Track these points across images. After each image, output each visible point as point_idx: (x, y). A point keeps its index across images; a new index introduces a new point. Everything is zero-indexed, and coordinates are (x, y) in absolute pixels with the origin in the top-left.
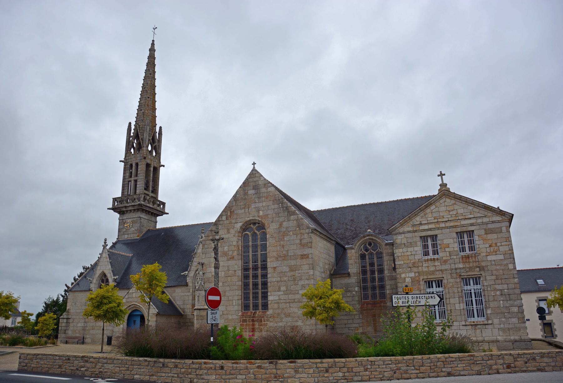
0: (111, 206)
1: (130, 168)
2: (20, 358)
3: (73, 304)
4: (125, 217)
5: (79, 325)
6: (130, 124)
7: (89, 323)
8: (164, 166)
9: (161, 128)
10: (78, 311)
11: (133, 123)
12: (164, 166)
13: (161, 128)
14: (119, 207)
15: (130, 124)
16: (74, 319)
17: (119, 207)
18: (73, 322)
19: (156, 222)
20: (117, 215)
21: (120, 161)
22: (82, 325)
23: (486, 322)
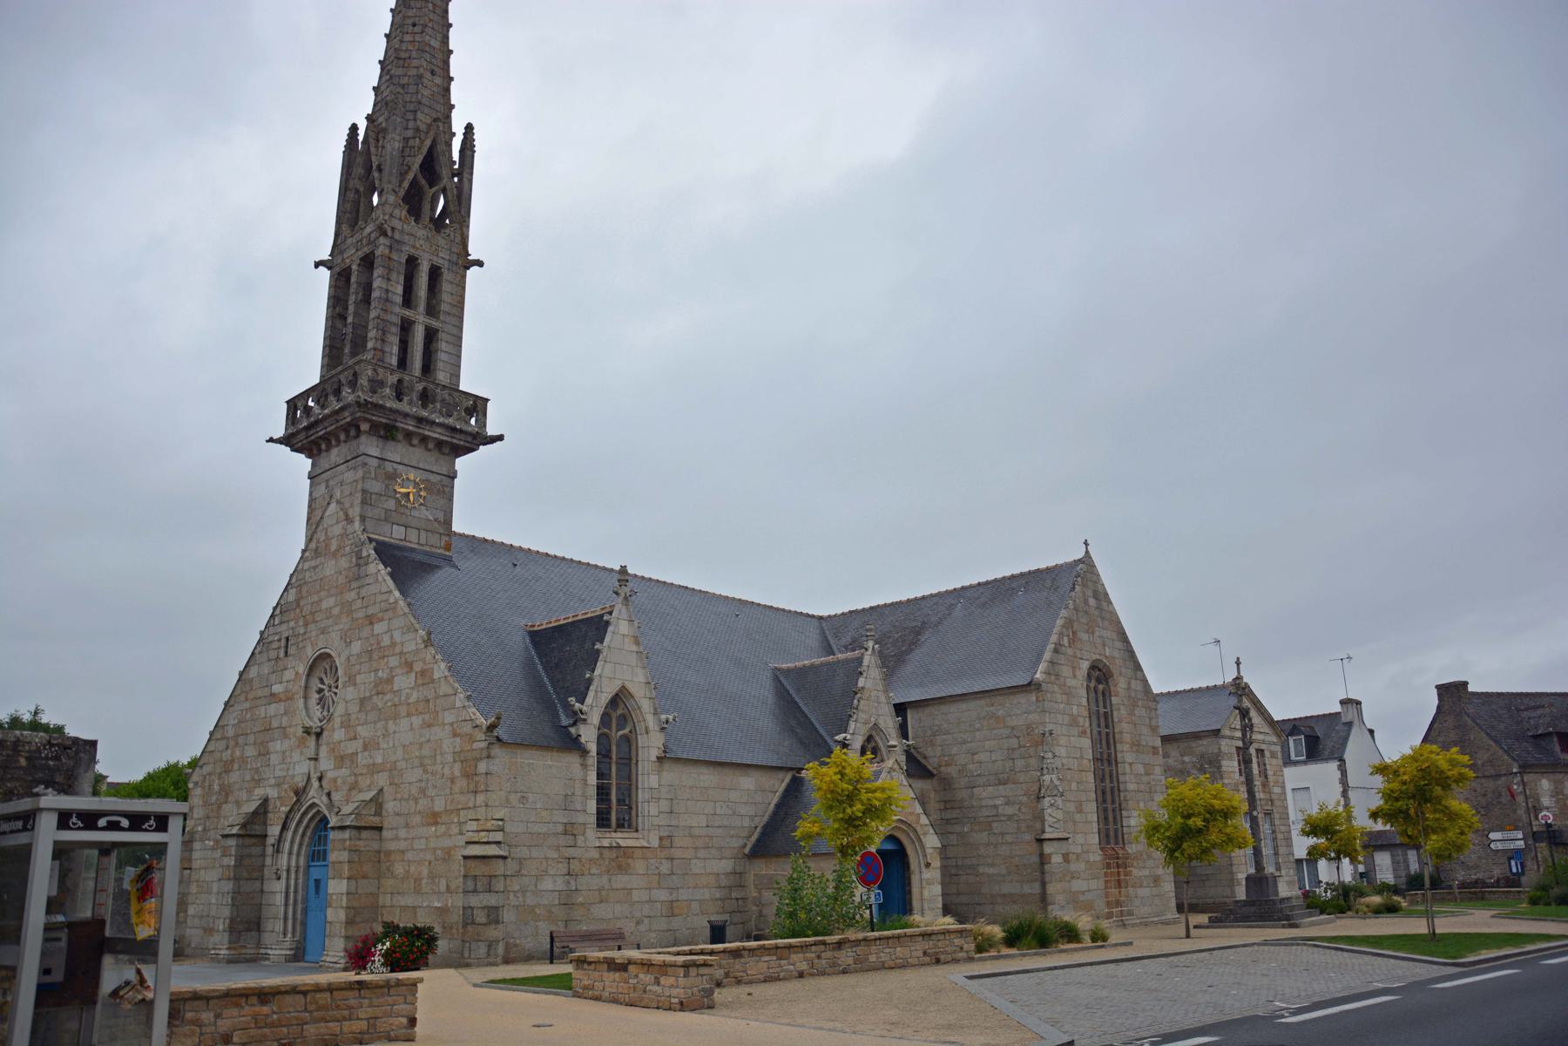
0: (280, 432)
1: (350, 279)
2: (413, 1021)
3: (514, 798)
4: (325, 463)
5: (547, 884)
6: (354, 128)
7: (583, 880)
8: (480, 263)
9: (469, 128)
10: (536, 828)
11: (362, 126)
12: (480, 263)
13: (469, 128)
14: (309, 429)
15: (354, 128)
16: (521, 861)
17: (309, 429)
18: (518, 874)
19: (453, 476)
20: (303, 463)
21: (317, 265)
22: (560, 884)
23: (1249, 851)
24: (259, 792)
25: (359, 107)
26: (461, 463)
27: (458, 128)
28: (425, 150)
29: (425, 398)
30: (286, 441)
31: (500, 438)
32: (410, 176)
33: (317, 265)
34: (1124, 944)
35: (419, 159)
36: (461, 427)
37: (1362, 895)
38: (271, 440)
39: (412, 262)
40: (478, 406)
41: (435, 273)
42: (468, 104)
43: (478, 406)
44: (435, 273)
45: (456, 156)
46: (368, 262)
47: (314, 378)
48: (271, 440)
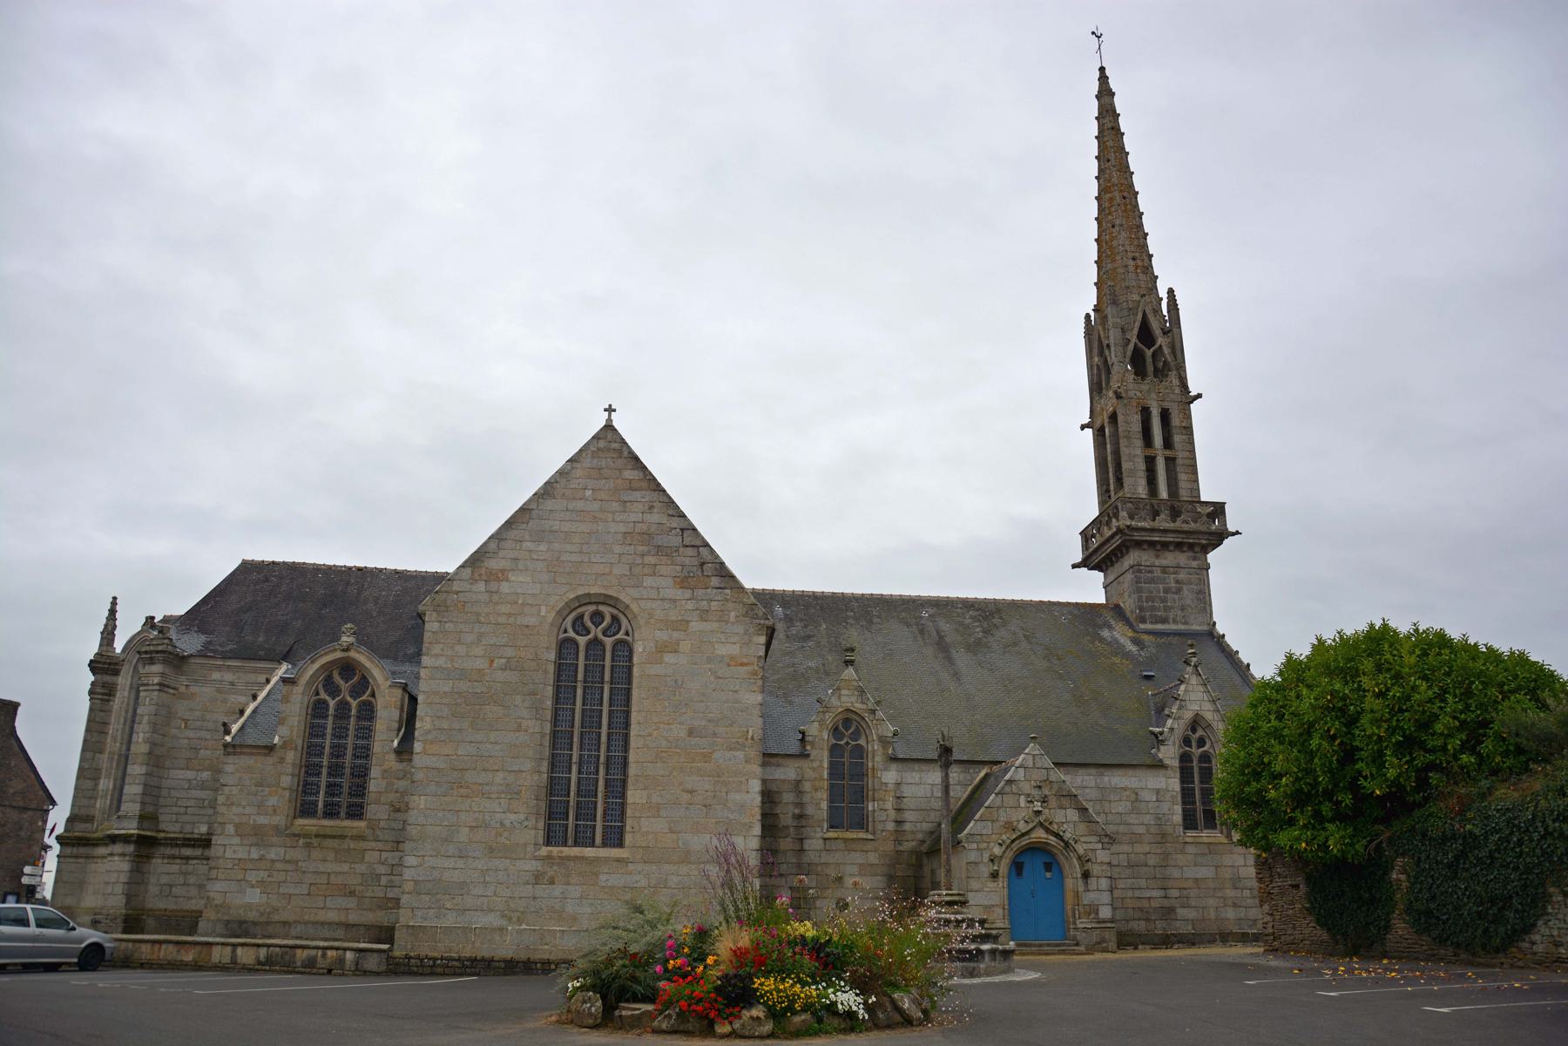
0: (1079, 558)
6: (1088, 316)
8: (1199, 396)
9: (1171, 292)
13: (1171, 292)
20: (1098, 576)
21: (1083, 427)
24: (1174, 726)
25: (1088, 300)
26: (1212, 557)
27: (1163, 293)
28: (1137, 325)
29: (1175, 514)
30: (1085, 563)
31: (1237, 533)
32: (1131, 346)
33: (1083, 427)
34: (325, 836)
35: (1136, 331)
36: (1207, 528)
37: (276, 828)
38: (1074, 566)
39: (1145, 412)
40: (1218, 510)
41: (1165, 416)
42: (1167, 275)
43: (1218, 510)
44: (1165, 416)
45: (1165, 312)
46: (1113, 418)
47: (1094, 512)
48: (1074, 566)
